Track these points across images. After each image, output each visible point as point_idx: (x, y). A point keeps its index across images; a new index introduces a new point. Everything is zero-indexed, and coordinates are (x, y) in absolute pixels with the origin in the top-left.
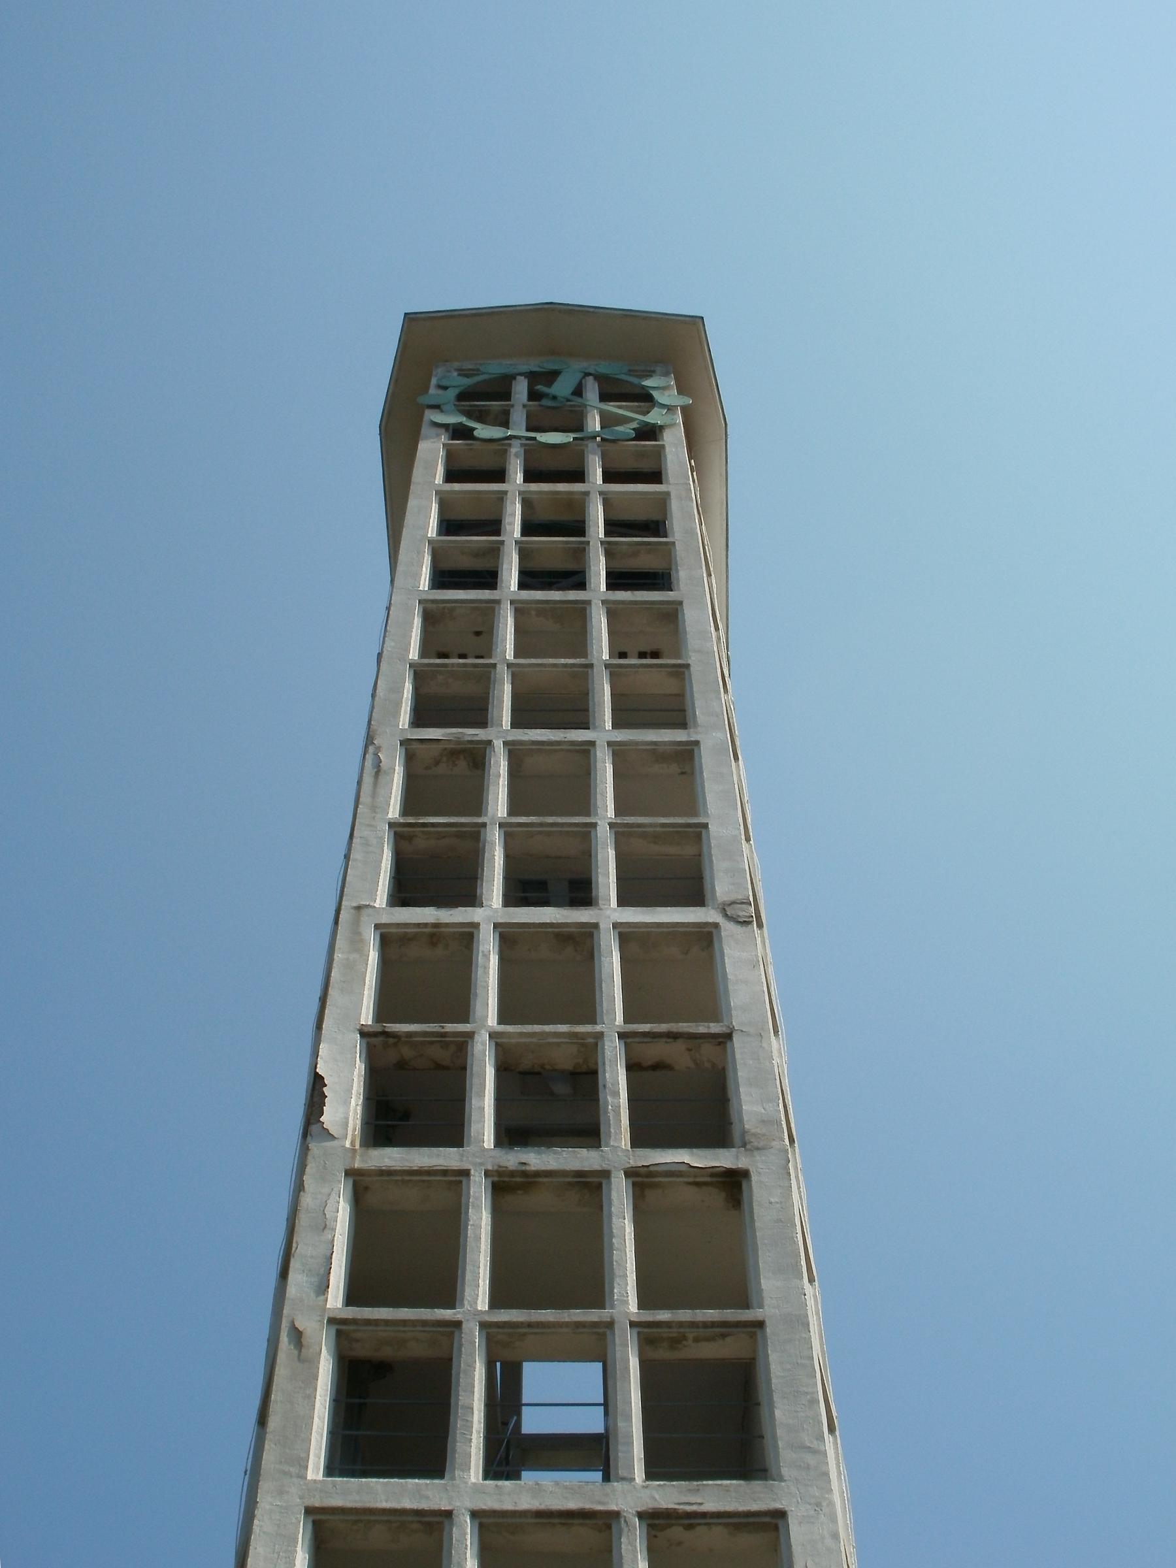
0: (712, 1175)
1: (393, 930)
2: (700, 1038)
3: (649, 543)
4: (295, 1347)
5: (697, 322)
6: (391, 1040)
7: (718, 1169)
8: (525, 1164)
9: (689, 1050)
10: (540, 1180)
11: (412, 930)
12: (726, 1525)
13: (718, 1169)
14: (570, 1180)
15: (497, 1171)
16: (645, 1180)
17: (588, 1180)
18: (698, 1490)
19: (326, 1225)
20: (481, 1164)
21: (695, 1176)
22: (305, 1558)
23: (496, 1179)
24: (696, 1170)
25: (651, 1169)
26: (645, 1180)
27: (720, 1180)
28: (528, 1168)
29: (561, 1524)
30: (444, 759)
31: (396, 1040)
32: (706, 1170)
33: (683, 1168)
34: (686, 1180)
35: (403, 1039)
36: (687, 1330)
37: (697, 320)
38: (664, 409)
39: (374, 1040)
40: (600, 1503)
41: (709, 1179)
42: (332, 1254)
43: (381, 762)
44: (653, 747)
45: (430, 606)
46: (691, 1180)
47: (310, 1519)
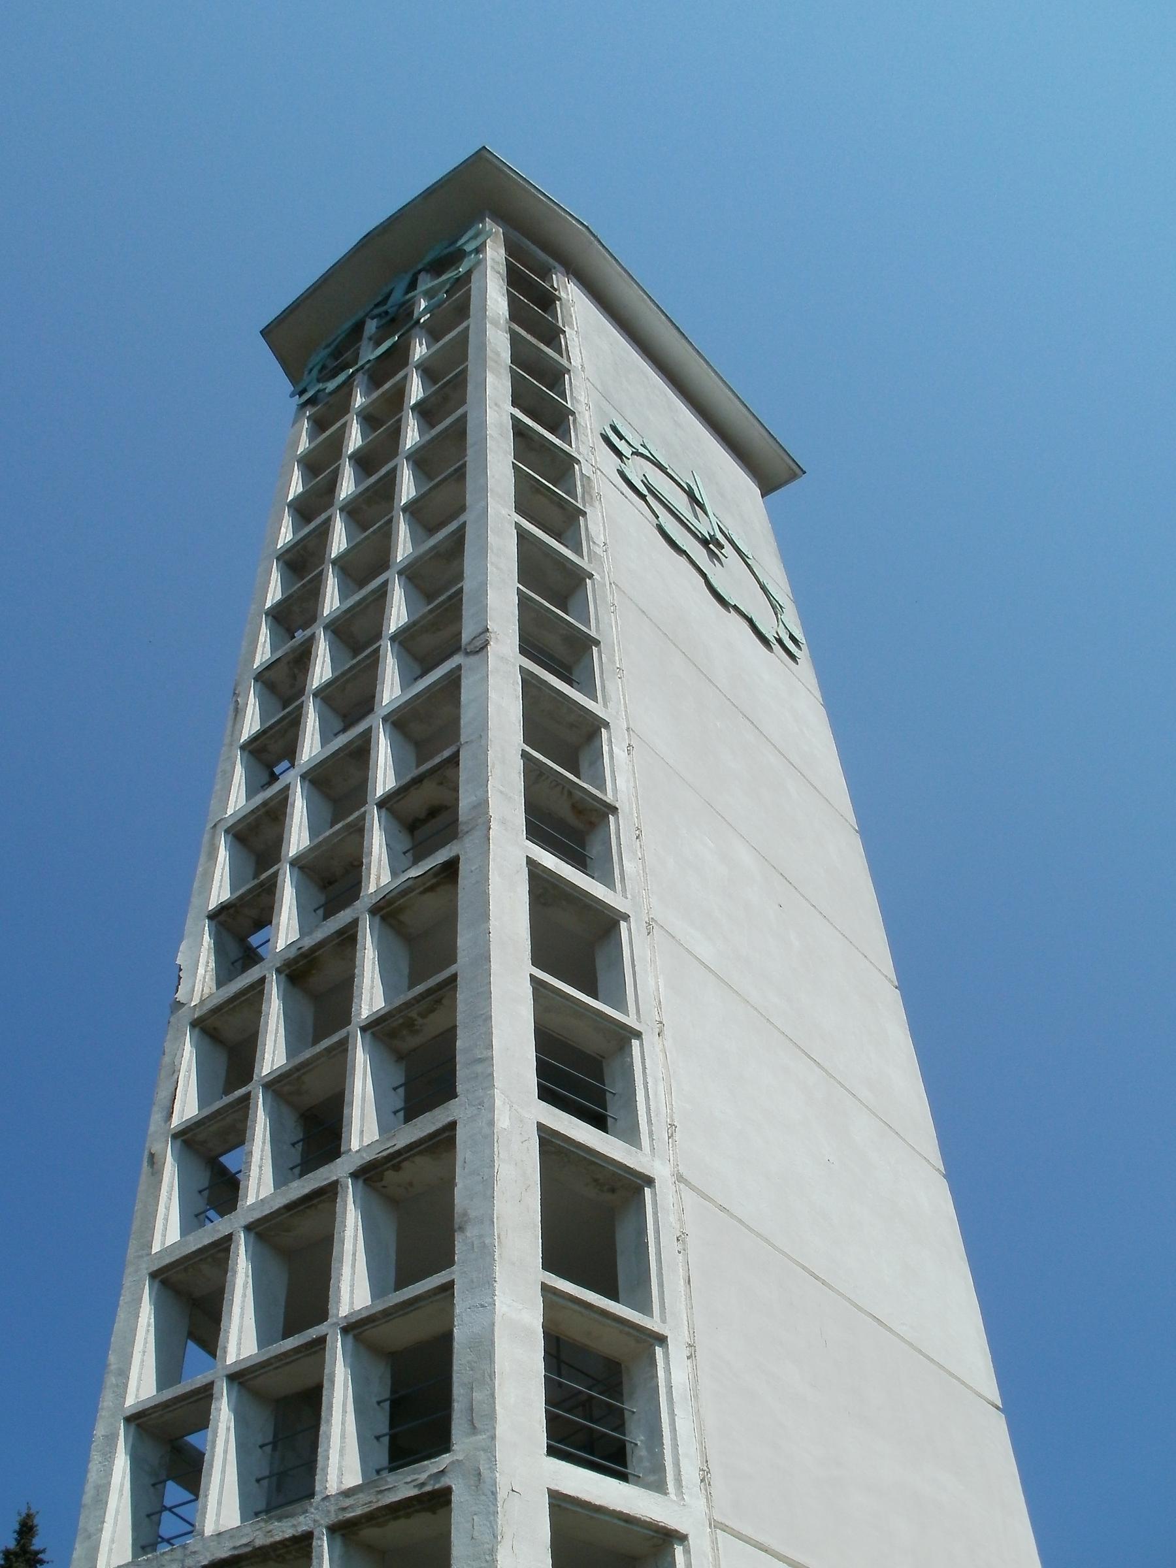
0: (436, 875)
1: (240, 827)
2: (439, 769)
3: (449, 382)
4: (151, 1168)
5: (481, 157)
6: (232, 911)
7: (434, 869)
8: (300, 948)
9: (441, 784)
10: (317, 954)
11: (251, 819)
12: (420, 1153)
13: (434, 869)
14: (337, 941)
15: (284, 965)
16: (388, 909)
17: (349, 933)
18: (394, 1135)
19: (175, 1070)
20: (273, 966)
21: (424, 884)
22: (151, 1309)
23: (287, 971)
24: (420, 878)
25: (387, 897)
26: (388, 909)
27: (442, 876)
28: (303, 950)
29: (306, 1208)
30: (296, 671)
31: (233, 909)
32: (427, 875)
33: (410, 883)
34: (417, 891)
35: (238, 905)
36: (406, 1012)
37: (482, 152)
38: (471, 255)
39: (222, 918)
40: (325, 1179)
41: (434, 881)
42: (176, 1089)
43: (239, 704)
44: (435, 551)
45: (287, 557)
46: (421, 889)
47: (157, 1281)
